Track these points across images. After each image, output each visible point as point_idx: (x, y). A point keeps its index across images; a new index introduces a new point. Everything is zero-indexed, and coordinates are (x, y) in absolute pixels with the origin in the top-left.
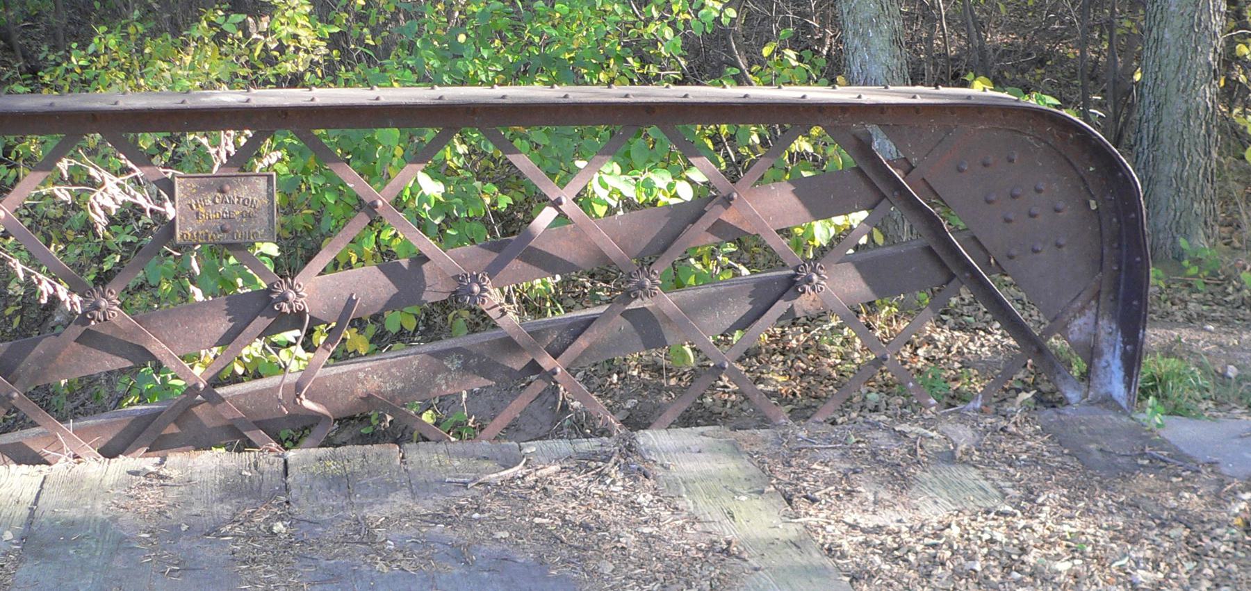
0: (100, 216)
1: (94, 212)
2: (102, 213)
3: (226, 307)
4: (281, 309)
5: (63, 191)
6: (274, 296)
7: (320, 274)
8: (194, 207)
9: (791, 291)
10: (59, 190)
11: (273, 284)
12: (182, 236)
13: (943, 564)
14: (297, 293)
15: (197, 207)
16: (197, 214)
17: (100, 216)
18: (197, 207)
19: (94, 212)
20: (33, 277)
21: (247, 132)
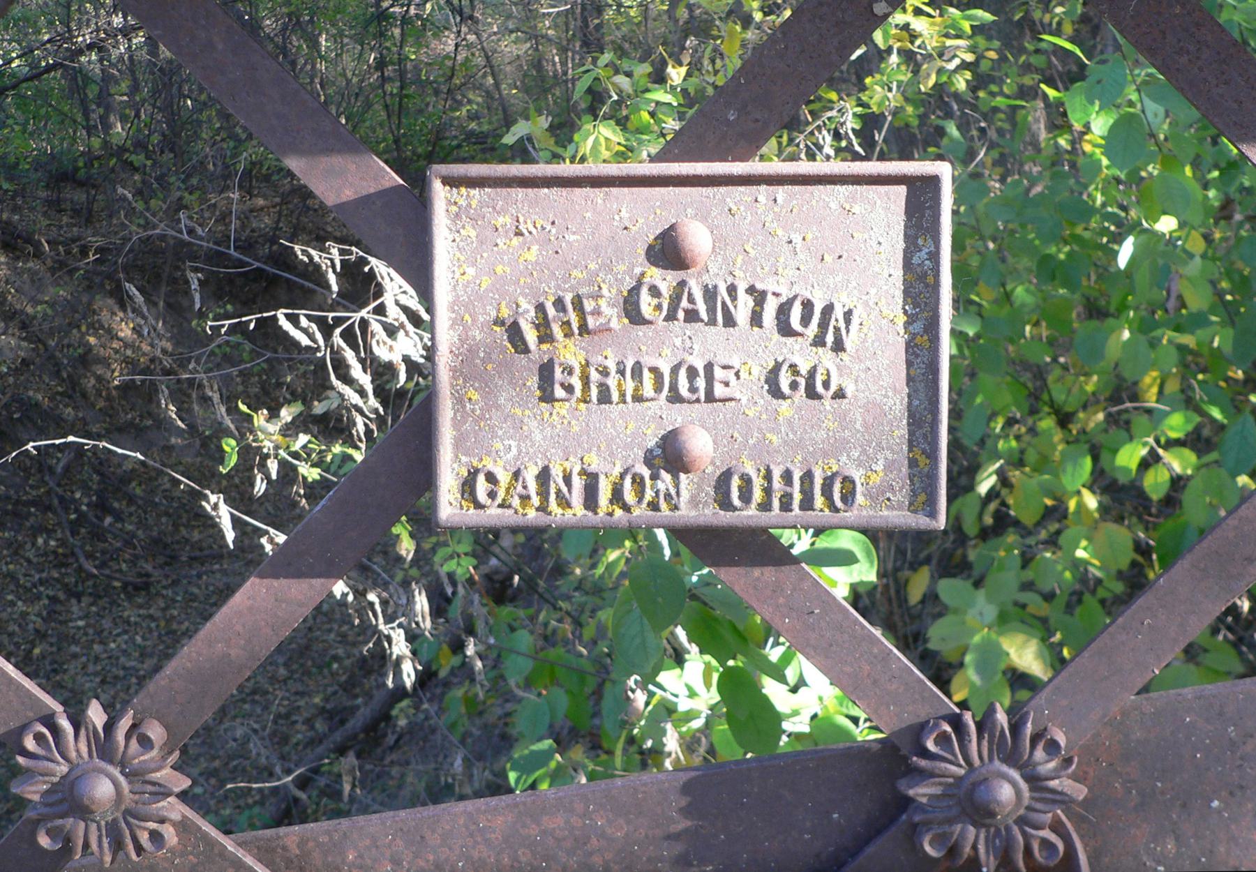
0: (362, 393)
1: (348, 380)
2: (365, 380)
3: (682, 824)
4: (953, 851)
5: (304, 322)
6: (922, 792)
7: (1138, 693)
8: (531, 336)
9: (1246, 494)
10: (293, 319)
11: (920, 730)
12: (468, 487)
13: (778, 452)
14: (1034, 780)
15: (545, 337)
16: (546, 372)
17: (362, 393)
18: (545, 337)
19: (348, 380)
20: (264, 540)
21: (631, 683)
